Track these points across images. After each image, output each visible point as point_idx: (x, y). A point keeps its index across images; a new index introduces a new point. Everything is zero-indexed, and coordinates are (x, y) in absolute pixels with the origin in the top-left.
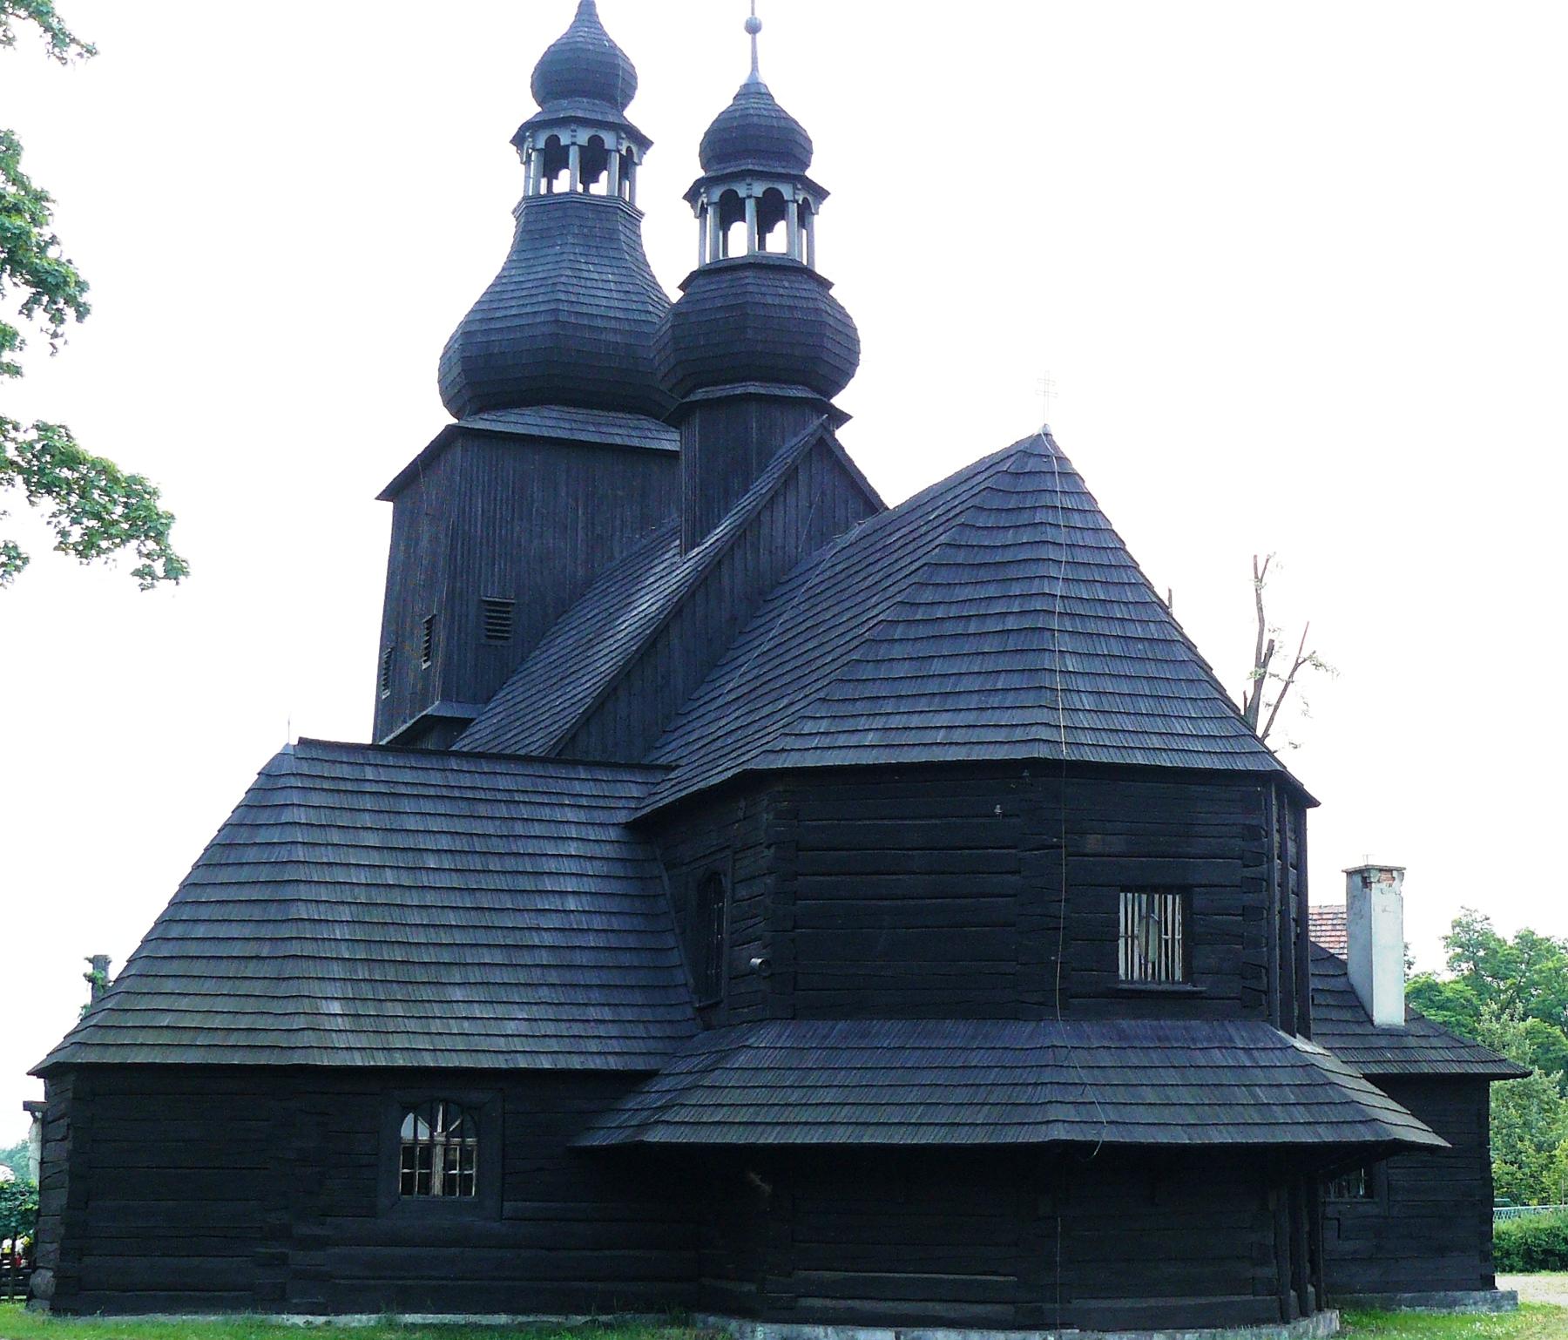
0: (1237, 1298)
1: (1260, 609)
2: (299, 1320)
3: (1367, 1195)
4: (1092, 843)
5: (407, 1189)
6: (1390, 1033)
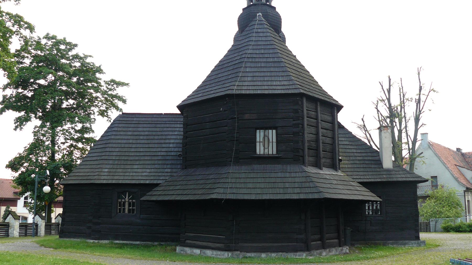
0: (289, 244)
1: (419, 80)
2: (92, 241)
3: (381, 214)
4: (247, 116)
5: (120, 212)
6: (388, 170)
